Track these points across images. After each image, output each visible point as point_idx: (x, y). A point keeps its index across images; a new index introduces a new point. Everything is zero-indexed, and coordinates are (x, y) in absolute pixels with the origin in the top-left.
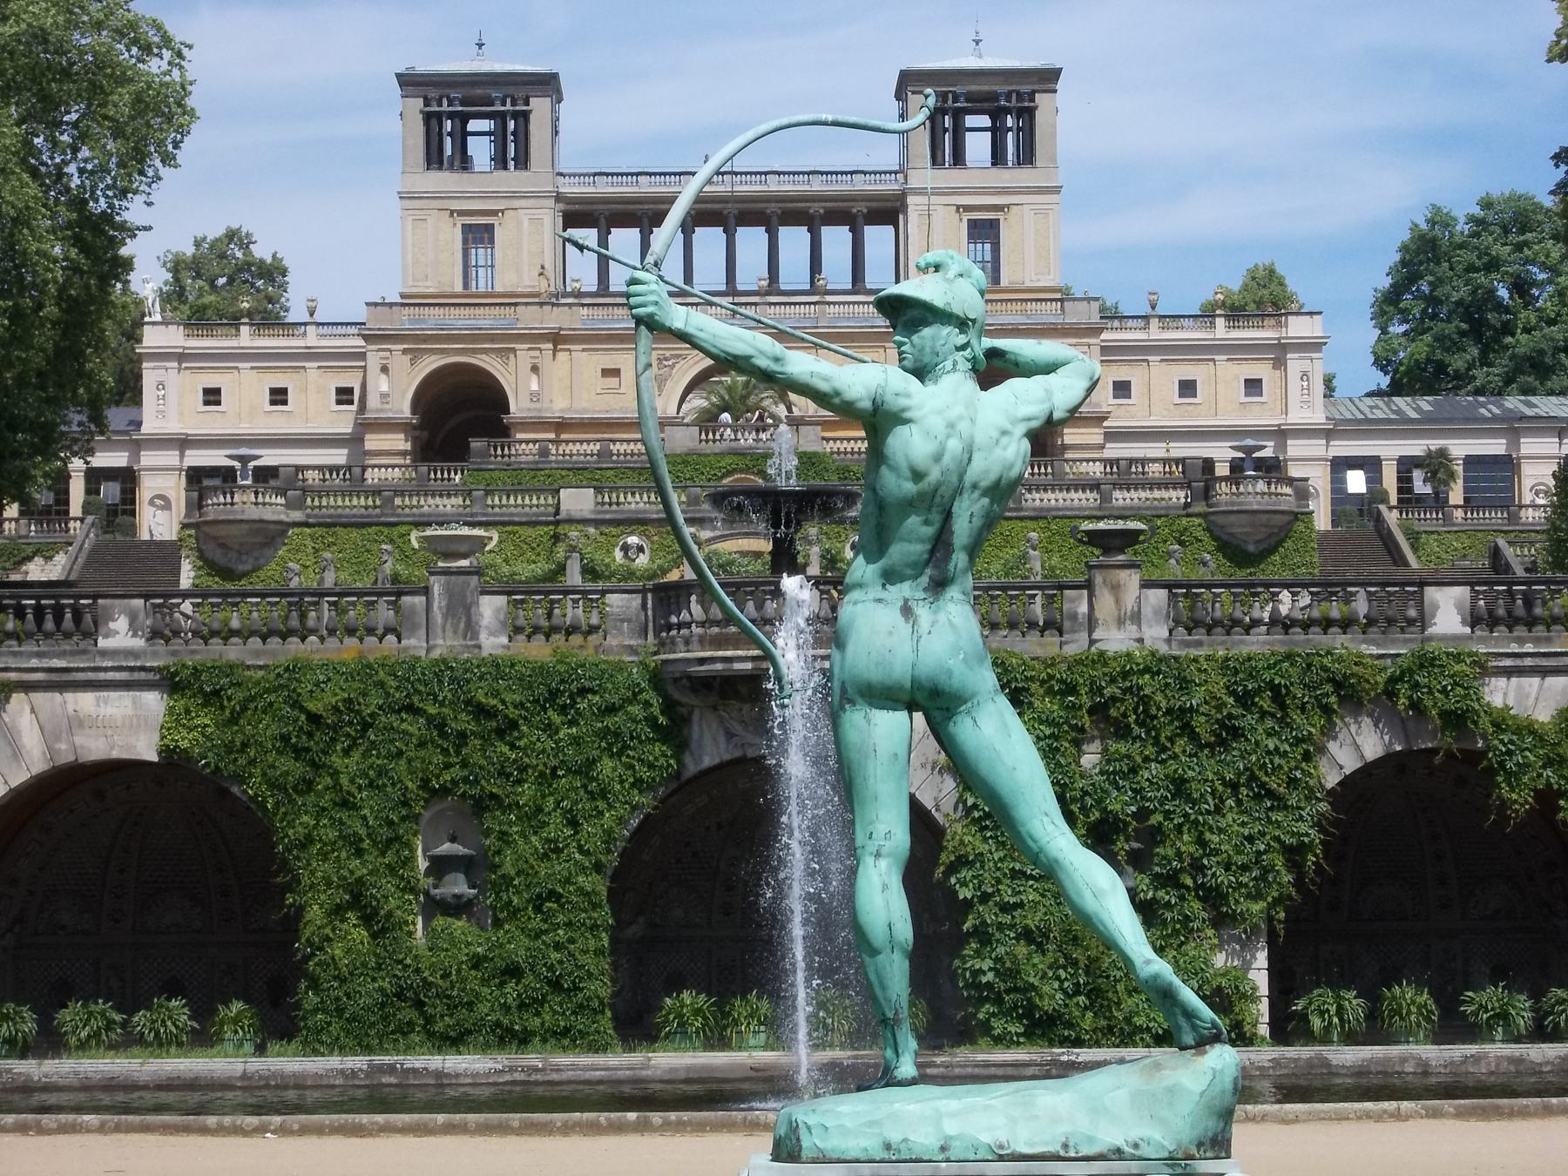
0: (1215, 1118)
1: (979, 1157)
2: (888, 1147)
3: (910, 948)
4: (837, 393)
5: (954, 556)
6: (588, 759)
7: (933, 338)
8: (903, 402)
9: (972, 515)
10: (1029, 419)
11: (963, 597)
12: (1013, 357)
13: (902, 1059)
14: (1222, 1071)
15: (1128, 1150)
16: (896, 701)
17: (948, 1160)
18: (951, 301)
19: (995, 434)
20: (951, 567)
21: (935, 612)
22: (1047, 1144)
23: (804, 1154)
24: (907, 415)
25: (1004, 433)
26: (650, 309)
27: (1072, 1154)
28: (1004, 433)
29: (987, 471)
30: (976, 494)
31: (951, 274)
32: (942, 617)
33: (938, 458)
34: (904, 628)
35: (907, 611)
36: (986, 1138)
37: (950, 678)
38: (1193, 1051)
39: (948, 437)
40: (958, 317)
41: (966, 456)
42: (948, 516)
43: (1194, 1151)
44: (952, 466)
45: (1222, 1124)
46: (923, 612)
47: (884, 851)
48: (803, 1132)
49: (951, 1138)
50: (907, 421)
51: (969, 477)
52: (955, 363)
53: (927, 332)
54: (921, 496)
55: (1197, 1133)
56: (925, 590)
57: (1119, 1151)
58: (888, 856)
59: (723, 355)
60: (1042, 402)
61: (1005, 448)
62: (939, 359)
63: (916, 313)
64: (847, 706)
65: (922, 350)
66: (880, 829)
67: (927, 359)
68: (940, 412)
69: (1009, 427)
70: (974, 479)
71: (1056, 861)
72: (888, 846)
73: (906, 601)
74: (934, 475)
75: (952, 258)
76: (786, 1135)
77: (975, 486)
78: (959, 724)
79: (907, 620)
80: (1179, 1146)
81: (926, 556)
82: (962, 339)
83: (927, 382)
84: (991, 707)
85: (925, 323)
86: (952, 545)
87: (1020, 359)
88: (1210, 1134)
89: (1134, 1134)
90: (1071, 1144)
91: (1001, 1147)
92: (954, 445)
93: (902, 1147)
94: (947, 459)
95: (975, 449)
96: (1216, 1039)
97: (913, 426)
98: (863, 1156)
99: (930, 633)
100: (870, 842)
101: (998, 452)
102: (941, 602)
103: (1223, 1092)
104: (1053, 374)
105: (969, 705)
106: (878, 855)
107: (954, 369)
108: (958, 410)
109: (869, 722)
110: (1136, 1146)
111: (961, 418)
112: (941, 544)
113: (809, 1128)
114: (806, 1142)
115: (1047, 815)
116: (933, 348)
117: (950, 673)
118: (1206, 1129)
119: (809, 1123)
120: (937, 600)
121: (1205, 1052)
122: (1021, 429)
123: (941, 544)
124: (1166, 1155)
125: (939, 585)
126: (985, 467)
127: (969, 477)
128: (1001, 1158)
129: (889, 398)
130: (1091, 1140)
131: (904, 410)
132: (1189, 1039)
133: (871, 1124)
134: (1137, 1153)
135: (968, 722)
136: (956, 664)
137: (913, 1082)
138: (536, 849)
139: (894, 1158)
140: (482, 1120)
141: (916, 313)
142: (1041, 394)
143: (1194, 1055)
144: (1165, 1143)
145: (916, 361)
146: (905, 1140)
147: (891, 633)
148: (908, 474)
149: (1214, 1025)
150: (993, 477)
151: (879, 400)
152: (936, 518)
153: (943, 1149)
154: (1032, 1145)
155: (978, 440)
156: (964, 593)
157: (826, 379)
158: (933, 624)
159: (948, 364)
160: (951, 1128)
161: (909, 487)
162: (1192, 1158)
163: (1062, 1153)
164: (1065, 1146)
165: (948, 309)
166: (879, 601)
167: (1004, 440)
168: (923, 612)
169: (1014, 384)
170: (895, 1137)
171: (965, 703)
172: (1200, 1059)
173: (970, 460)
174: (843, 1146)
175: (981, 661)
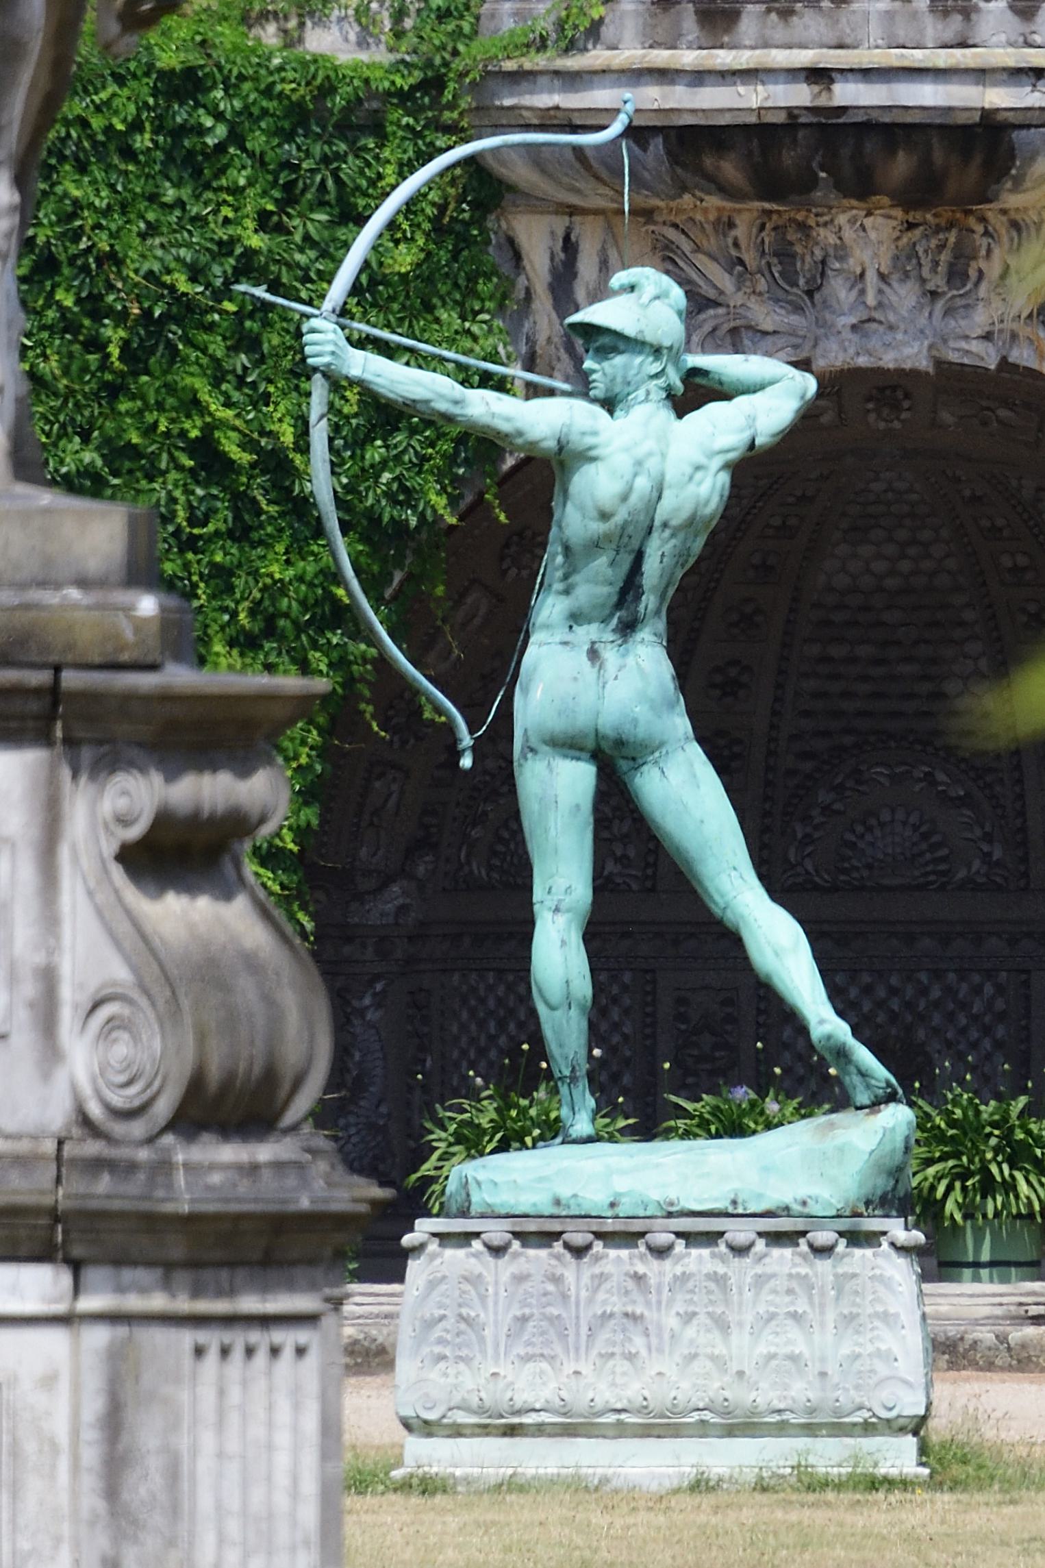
0: (884, 1176)
1: (648, 1213)
2: (557, 1202)
3: (589, 1003)
4: (520, 434)
5: (644, 598)
6: (605, 1312)
7: (626, 367)
8: (589, 441)
9: (663, 555)
10: (728, 451)
11: (655, 639)
12: (717, 377)
13: (577, 1116)
14: (893, 1129)
15: (797, 1208)
16: (581, 749)
17: (617, 1217)
18: (643, 327)
19: (689, 470)
20: (641, 608)
21: (624, 656)
22: (716, 1200)
23: (473, 1212)
24: (593, 453)
25: (698, 468)
26: (326, 359)
27: (740, 1211)
28: (698, 468)
29: (677, 510)
30: (667, 533)
31: (645, 299)
32: (630, 660)
33: (625, 498)
34: (979, 332)
35: (593, 654)
36: (656, 1195)
37: (635, 727)
38: (867, 1110)
39: (635, 475)
40: (652, 346)
41: (655, 494)
42: (639, 557)
43: (862, 1209)
44: (640, 505)
45: (892, 1182)
46: (610, 655)
47: (563, 906)
48: (473, 1187)
49: (621, 1195)
50: (594, 459)
51: (664, 510)
52: (648, 393)
53: (619, 360)
54: (608, 537)
55: (865, 1191)
56: (613, 630)
57: (787, 1208)
58: (568, 911)
59: (400, 400)
60: (742, 430)
61: (699, 484)
62: (631, 389)
63: (605, 340)
64: (530, 755)
65: (613, 380)
66: (560, 883)
67: (617, 389)
68: (627, 450)
69: (703, 460)
70: (665, 518)
71: (742, 917)
72: (568, 901)
73: (593, 643)
74: (621, 516)
75: (647, 278)
76: (457, 1190)
77: (665, 525)
78: (645, 774)
79: (593, 664)
80: (847, 1203)
81: (615, 599)
82: (656, 367)
83: (618, 413)
84: (680, 757)
85: (615, 350)
86: (641, 586)
87: (724, 379)
88: (879, 1193)
89: (802, 1193)
90: (740, 1200)
91: (672, 1204)
92: (643, 484)
93: (572, 1202)
94: (634, 498)
95: (666, 485)
96: (891, 1098)
97: (599, 464)
98: (531, 1211)
99: (616, 678)
100: (549, 897)
101: (692, 488)
102: (630, 643)
103: (894, 1150)
104: (759, 394)
105: (657, 754)
106: (557, 910)
107: (647, 400)
108: (650, 445)
109: (551, 771)
110: (804, 1203)
111: (650, 454)
112: (630, 588)
113: (479, 1184)
114: (475, 1198)
115: (735, 869)
116: (625, 377)
117: (635, 722)
118: (875, 1187)
119: (480, 1178)
120: (625, 642)
121: (879, 1111)
122: (718, 461)
123: (630, 588)
124: (834, 1213)
125: (628, 628)
126: (675, 505)
127: (664, 510)
128: (670, 1215)
129: (574, 437)
130: (760, 1196)
131: (590, 448)
132: (863, 1098)
133: (541, 1179)
134: (806, 1211)
135: (655, 772)
136: (641, 711)
137: (589, 1140)
138: (208, 249)
139: (564, 1213)
140: (527, 97)
141: (605, 340)
142: (741, 421)
143: (867, 1114)
144: (833, 1201)
145: (607, 390)
146: (575, 1196)
147: (575, 679)
148: (595, 514)
149: (889, 1084)
150: (684, 515)
151: (564, 441)
152: (626, 561)
153: (612, 1205)
154: (700, 1202)
155: (668, 478)
156: (655, 634)
157: (508, 419)
158: (621, 668)
159: (641, 393)
160: (621, 1185)
161: (598, 527)
162: (860, 1215)
163: (731, 1210)
164: (734, 1203)
165: (640, 337)
166: (565, 643)
167: (699, 475)
168: (610, 655)
169: (713, 409)
170: (565, 1192)
171: (653, 753)
172: (872, 1118)
173: (660, 498)
174: (512, 1202)
175: (671, 706)
